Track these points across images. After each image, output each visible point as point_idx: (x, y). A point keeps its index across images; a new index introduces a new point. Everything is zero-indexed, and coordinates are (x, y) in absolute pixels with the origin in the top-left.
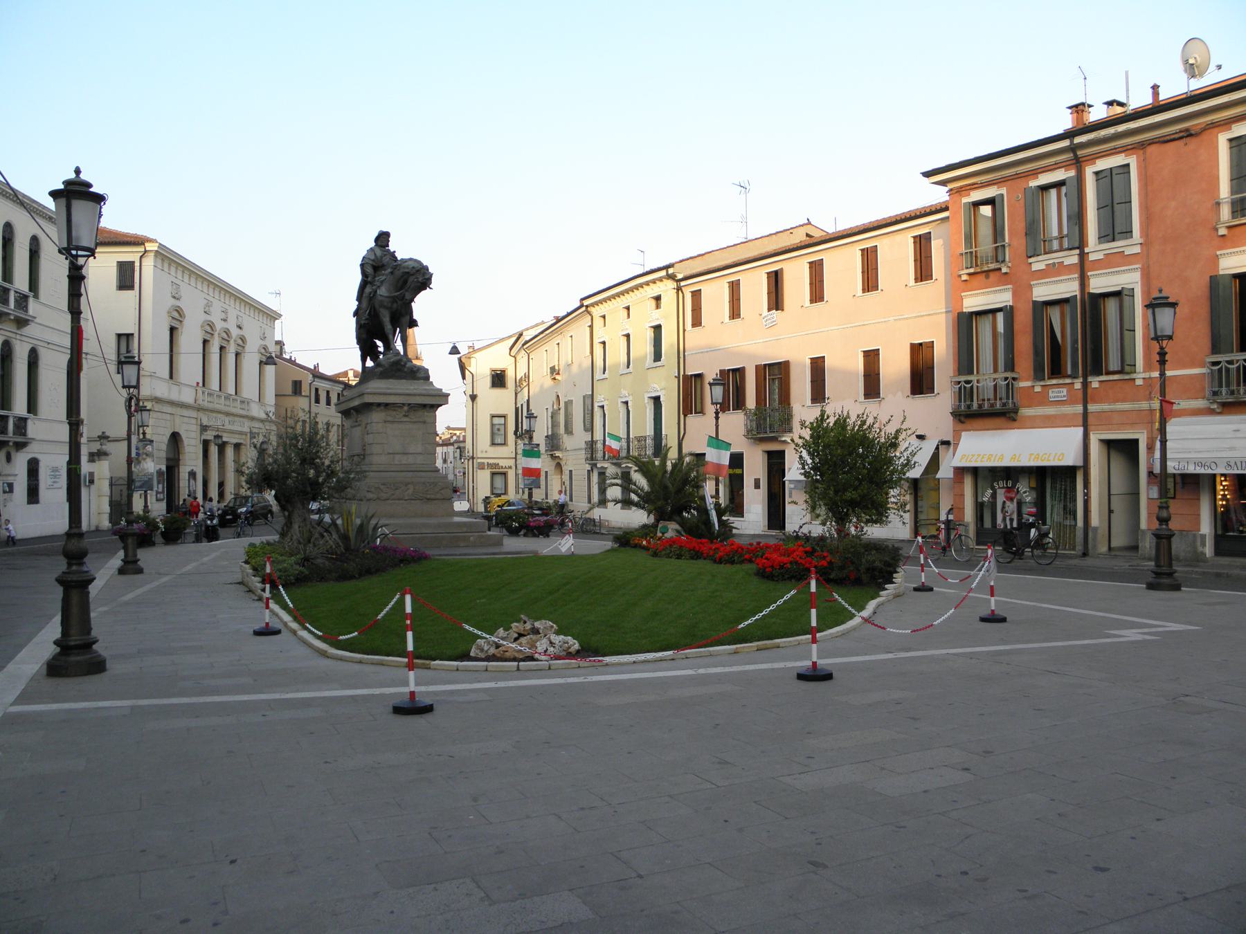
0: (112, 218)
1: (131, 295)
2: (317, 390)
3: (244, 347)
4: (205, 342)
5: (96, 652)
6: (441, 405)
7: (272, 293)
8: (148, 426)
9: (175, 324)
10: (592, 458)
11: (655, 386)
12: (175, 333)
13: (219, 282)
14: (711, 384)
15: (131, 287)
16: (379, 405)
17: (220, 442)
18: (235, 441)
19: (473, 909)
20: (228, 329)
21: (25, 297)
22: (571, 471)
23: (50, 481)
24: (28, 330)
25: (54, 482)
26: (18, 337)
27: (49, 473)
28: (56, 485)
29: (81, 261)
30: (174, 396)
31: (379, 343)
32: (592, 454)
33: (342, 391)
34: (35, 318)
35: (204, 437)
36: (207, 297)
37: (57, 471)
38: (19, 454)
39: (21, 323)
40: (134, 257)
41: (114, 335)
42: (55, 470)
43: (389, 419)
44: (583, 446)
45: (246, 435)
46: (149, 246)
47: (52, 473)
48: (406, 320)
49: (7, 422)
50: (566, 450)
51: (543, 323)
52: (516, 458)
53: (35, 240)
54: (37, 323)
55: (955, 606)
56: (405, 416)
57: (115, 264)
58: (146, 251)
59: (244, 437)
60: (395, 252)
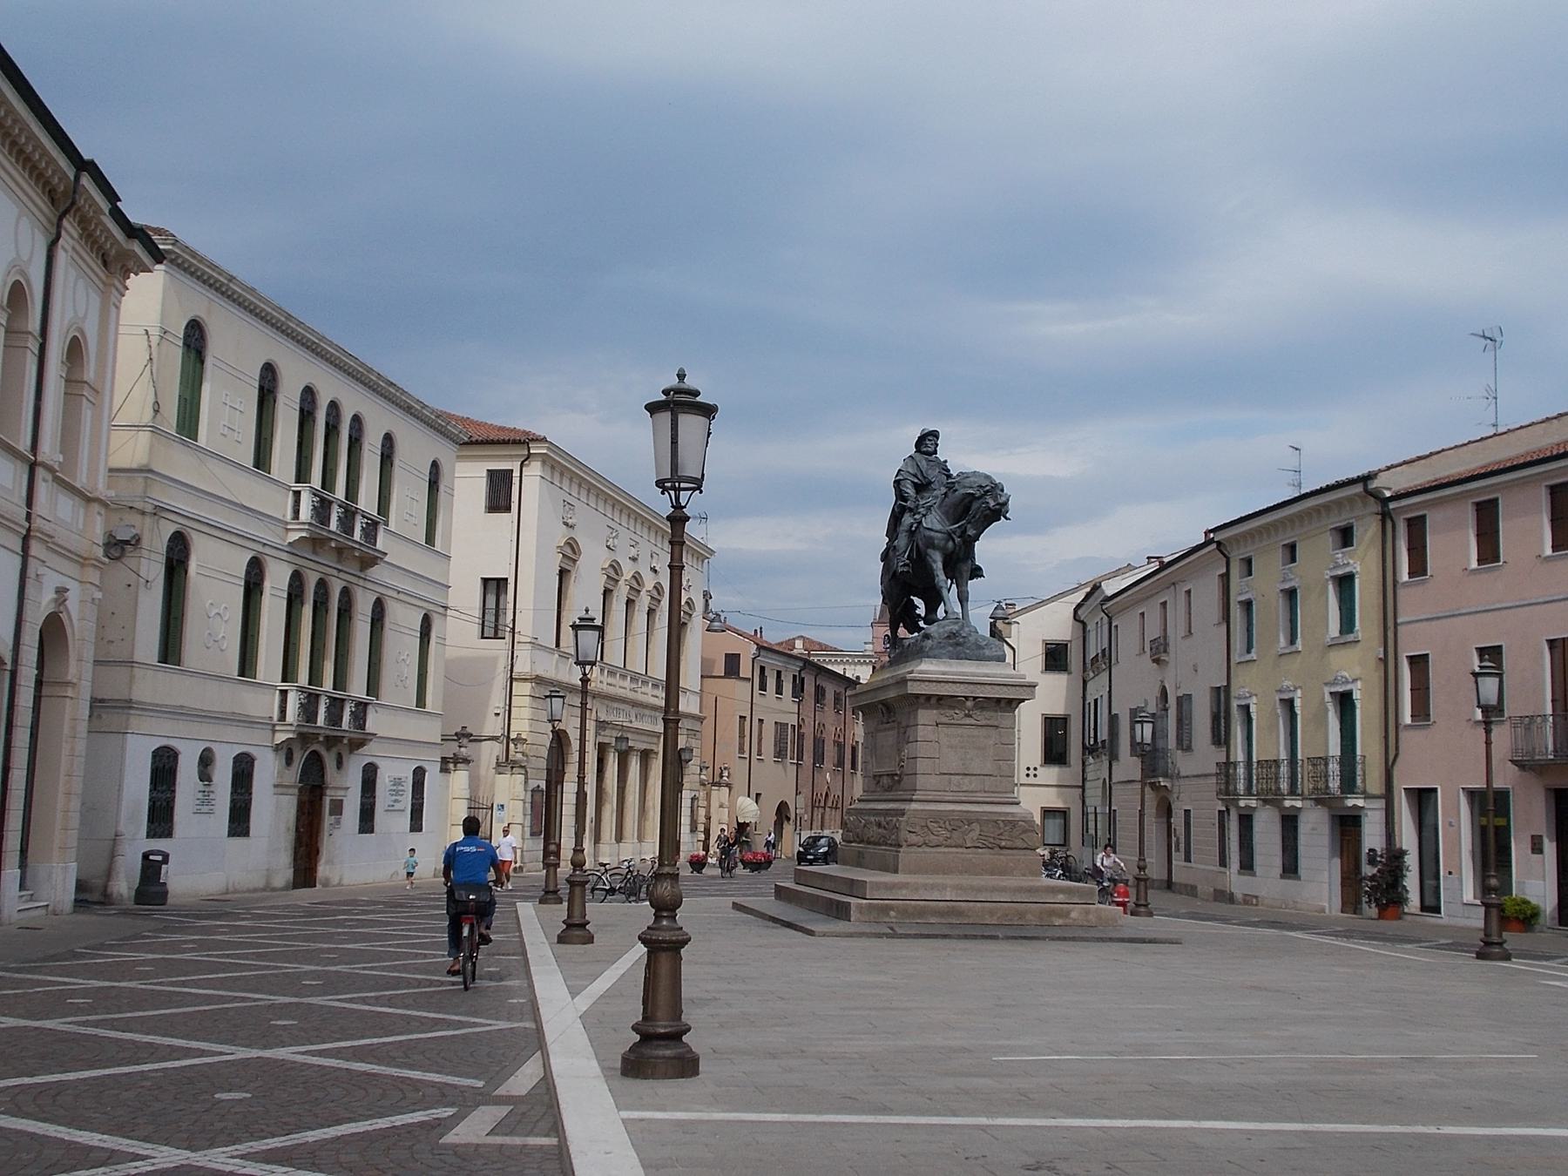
1: (505, 520)
2: (762, 669)
5: (686, 1045)
6: (1023, 700)
8: (560, 721)
10: (1227, 791)
11: (1346, 674)
14: (574, 627)
15: (508, 509)
16: (929, 697)
17: (624, 748)
18: (643, 746)
21: (375, 524)
22: (1187, 812)
24: (375, 572)
25: (396, 801)
26: (361, 582)
28: (397, 806)
29: (684, 495)
31: (918, 601)
32: (1227, 783)
33: (800, 672)
35: (600, 739)
37: (400, 784)
41: (479, 580)
42: (398, 782)
43: (945, 720)
44: (1214, 769)
45: (659, 737)
47: (395, 788)
48: (966, 568)
50: (1179, 776)
51: (1130, 568)
52: (1083, 787)
53: (388, 440)
56: (966, 716)
58: (529, 455)
59: (655, 740)
60: (946, 461)
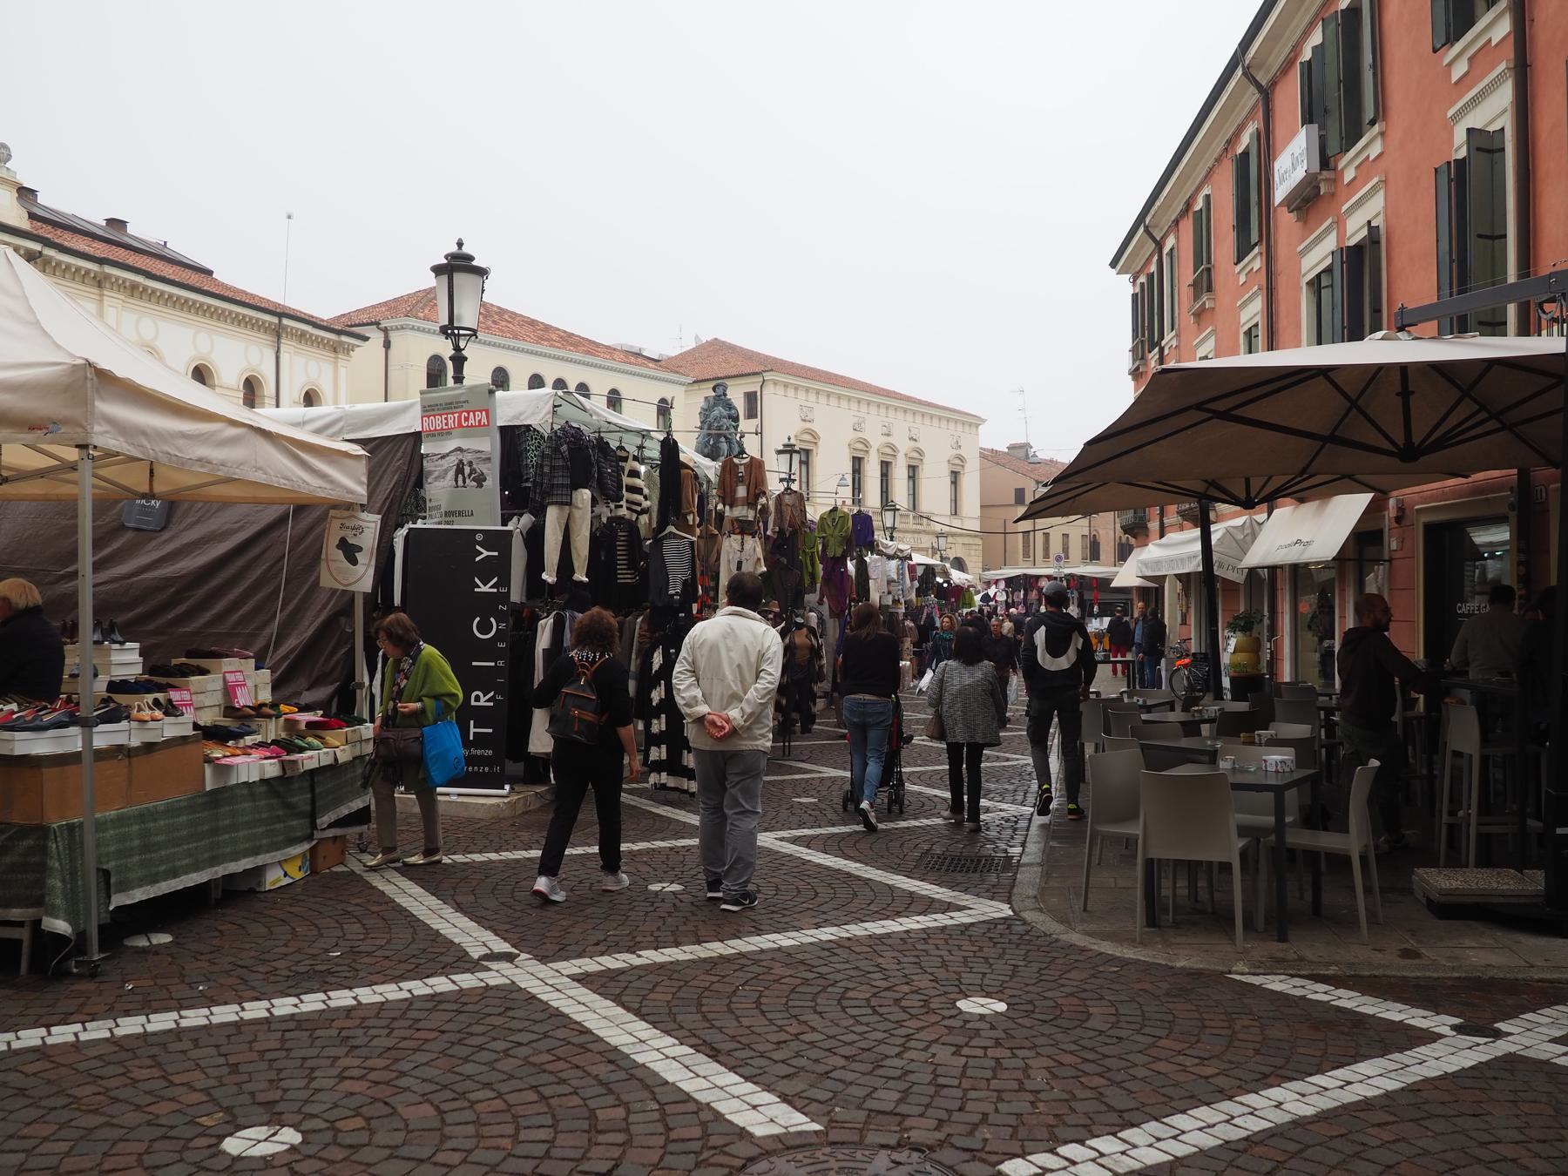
0: (497, 292)
3: (963, 466)
9: (956, 469)
19: (1000, 957)
55: (439, 866)
57: (742, 395)
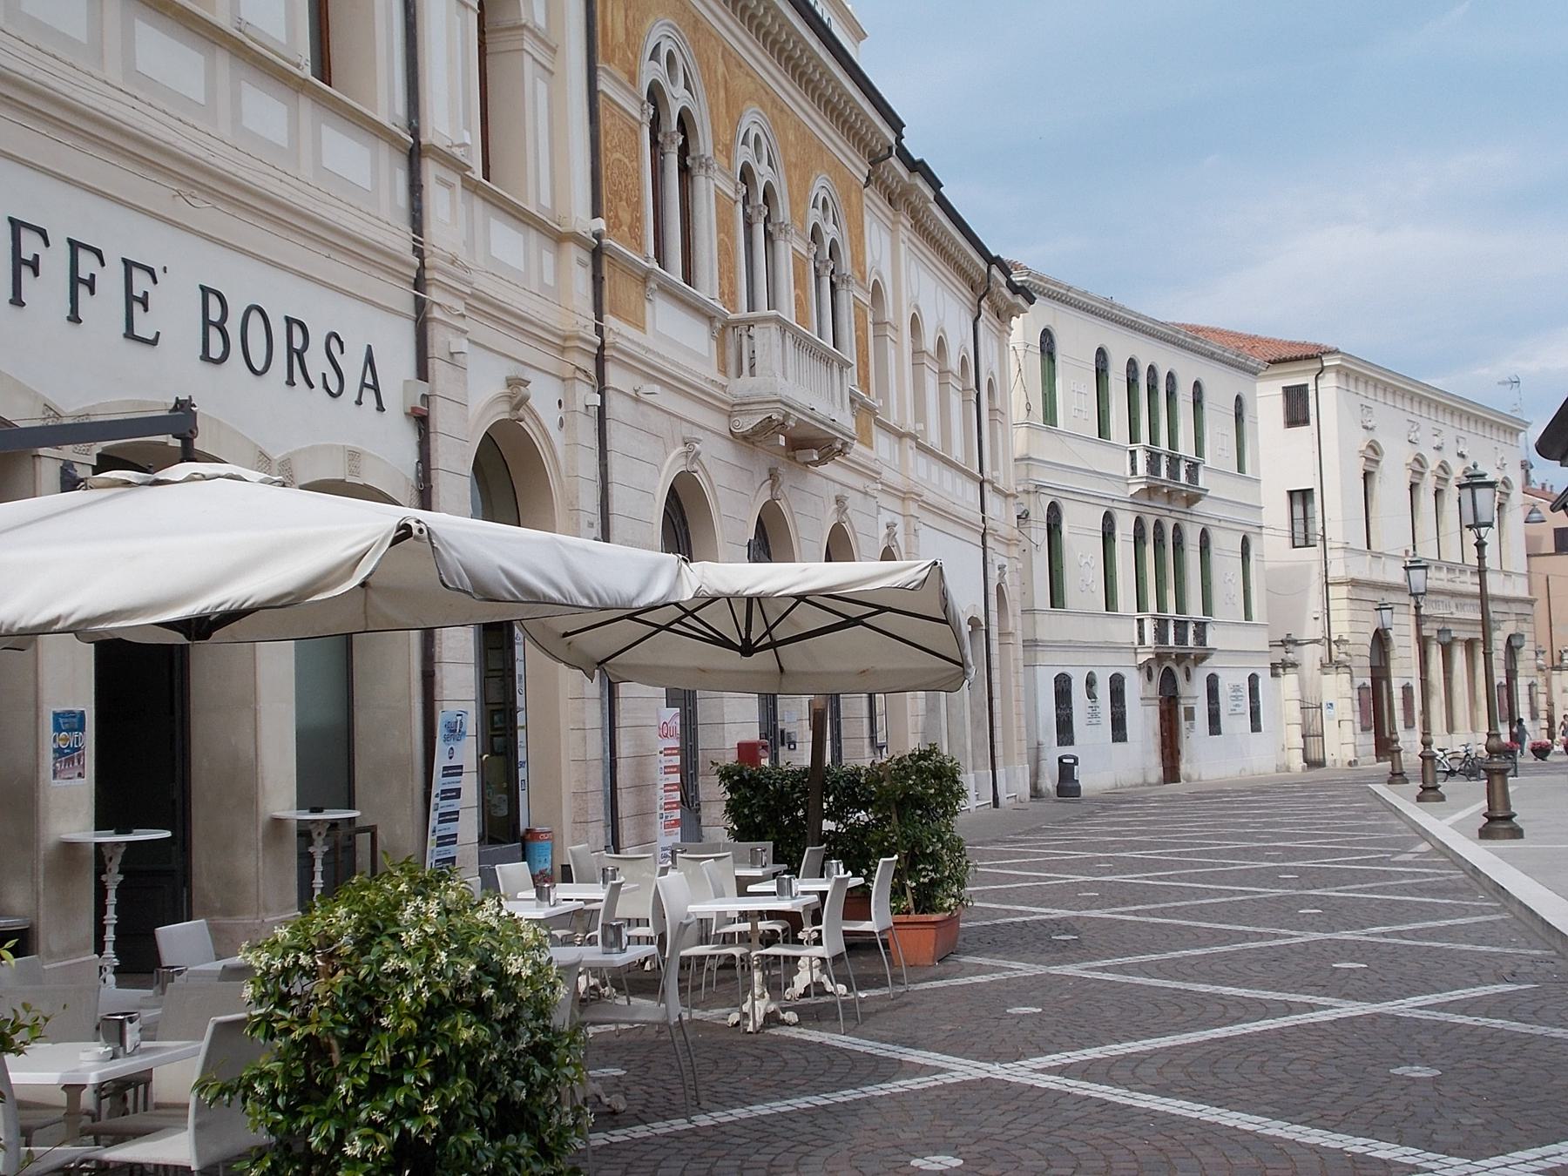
4: (1413, 487)
7: (1504, 383)
12: (1368, 477)
13: (1442, 397)
15: (1306, 422)
18: (1467, 636)
20: (1422, 456)
23: (1231, 705)
24: (1198, 507)
25: (1236, 705)
26: (1189, 518)
27: (1230, 694)
30: (1378, 577)
34: (1207, 490)
36: (1412, 418)
37: (1239, 690)
38: (1197, 669)
39: (1193, 499)
40: (1308, 380)
42: (1236, 688)
46: (1328, 361)
49: (1186, 629)
54: (1210, 497)
57: (1281, 391)
